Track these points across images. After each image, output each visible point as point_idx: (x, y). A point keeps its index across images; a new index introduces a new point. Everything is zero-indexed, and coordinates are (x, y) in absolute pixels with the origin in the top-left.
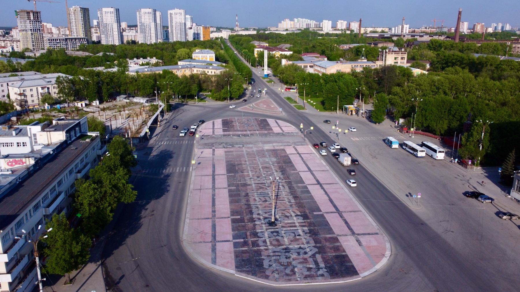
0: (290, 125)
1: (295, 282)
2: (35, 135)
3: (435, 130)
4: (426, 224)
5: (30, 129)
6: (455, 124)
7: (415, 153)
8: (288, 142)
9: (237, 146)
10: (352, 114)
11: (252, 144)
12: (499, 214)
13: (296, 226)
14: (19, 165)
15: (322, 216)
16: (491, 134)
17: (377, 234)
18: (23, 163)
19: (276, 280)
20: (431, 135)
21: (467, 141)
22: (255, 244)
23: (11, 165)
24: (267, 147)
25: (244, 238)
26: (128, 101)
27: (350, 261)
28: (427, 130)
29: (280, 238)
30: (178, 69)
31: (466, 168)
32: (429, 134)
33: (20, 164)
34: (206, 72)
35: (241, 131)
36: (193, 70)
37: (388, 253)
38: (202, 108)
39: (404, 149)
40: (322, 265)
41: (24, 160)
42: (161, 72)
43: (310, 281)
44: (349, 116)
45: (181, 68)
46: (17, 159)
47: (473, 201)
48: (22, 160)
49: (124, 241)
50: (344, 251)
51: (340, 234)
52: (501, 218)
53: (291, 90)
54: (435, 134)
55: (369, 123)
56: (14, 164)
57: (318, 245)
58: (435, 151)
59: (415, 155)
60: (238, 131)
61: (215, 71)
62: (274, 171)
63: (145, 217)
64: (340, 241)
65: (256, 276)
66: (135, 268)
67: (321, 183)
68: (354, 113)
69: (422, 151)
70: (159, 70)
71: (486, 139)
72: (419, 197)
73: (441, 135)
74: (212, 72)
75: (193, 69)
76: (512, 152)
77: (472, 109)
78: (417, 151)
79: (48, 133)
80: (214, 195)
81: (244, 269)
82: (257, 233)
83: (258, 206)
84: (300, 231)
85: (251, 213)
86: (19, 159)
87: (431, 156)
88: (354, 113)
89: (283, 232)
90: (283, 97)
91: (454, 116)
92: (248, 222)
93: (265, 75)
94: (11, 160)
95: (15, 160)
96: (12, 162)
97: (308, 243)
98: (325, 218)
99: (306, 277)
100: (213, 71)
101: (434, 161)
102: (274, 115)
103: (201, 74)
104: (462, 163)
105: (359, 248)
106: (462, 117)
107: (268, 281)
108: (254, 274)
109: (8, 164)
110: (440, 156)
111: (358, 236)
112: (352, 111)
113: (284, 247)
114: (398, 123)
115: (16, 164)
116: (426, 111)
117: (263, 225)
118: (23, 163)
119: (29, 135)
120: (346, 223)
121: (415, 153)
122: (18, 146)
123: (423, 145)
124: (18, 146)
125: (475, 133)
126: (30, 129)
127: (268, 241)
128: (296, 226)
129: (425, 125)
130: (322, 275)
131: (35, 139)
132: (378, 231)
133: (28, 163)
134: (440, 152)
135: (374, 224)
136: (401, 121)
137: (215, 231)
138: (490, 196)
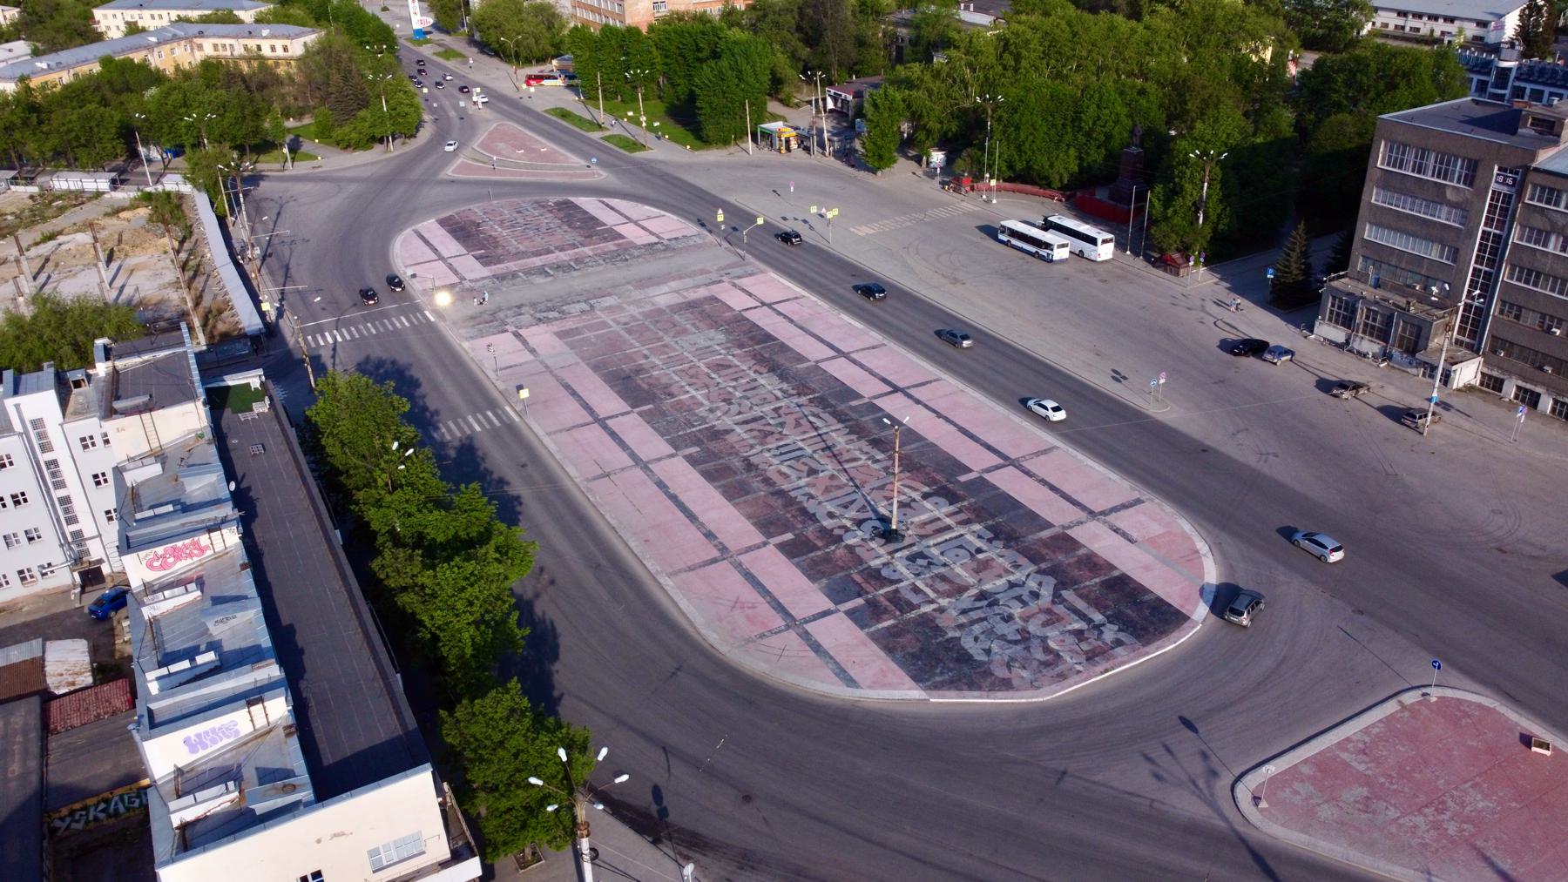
0: (656, 211)
1: (1076, 678)
2: (38, 424)
3: (1046, 178)
4: (1215, 451)
5: (17, 406)
6: (1096, 156)
7: (1043, 252)
8: (703, 272)
9: (575, 308)
10: (788, 149)
11: (610, 295)
12: (1325, 386)
13: (948, 528)
14: (189, 561)
15: (633, 406)
16: (1224, 183)
17: (1138, 501)
18: (202, 550)
19: (1033, 685)
20: (1036, 189)
21: (1166, 206)
22: (895, 598)
23: (162, 567)
24: (663, 297)
25: (859, 595)
26: (34, 189)
27: (1146, 591)
28: (1022, 177)
29: (942, 570)
30: (150, 47)
31: (1177, 274)
32: (1029, 187)
33: (191, 556)
34: (266, 52)
35: (537, 254)
36: (200, 47)
37: (1202, 546)
38: (328, 185)
39: (1001, 242)
40: (1098, 617)
41: (204, 539)
42: (96, 68)
43: (1107, 665)
44: (784, 157)
45: (159, 44)
46: (179, 544)
47: (1251, 362)
48: (196, 544)
49: (552, 687)
50: (1113, 567)
51: (1066, 522)
52: (1335, 396)
53: (546, 82)
54: (1049, 185)
55: (851, 170)
56: (171, 560)
57: (1043, 566)
58: (1093, 241)
59: (1041, 258)
60: (520, 255)
61: (287, 42)
62: (754, 376)
63: (537, 595)
64: (1082, 541)
65: (980, 688)
66: (663, 758)
67: (901, 385)
68: (794, 145)
69: (1063, 246)
70: (86, 61)
71: (1215, 198)
72: (1162, 381)
73: (1063, 188)
74: (273, 48)
75: (198, 41)
76: (1296, 229)
77: (1130, 116)
78: (1048, 246)
79: (146, 416)
80: (661, 485)
81: (938, 679)
82: (878, 571)
83: (807, 490)
84: (969, 537)
85: (812, 518)
86: (187, 541)
87: (1081, 254)
88: (794, 145)
89: (935, 552)
90: (539, 109)
91: (1088, 135)
92: (827, 546)
93: (418, 32)
94: (160, 550)
95: (174, 549)
96: (163, 556)
97: (1017, 566)
98: (995, 488)
99: (1091, 657)
100: (279, 44)
101: (1093, 266)
102: (575, 180)
103: (248, 60)
104: (1163, 262)
105: (1132, 547)
106: (1109, 137)
107: (1011, 693)
108: (973, 686)
109: (150, 566)
110: (1105, 251)
111: (1108, 518)
112: (788, 141)
113: (974, 591)
114: (928, 163)
115: (178, 558)
116: (1017, 128)
117: (873, 545)
118: (202, 550)
119: (18, 427)
120: (1043, 482)
121: (1043, 252)
122: (98, 483)
123: (1048, 226)
124: (98, 483)
125: (1188, 187)
126: (17, 406)
127: (920, 584)
128: (948, 528)
129: (1019, 166)
130: (1119, 643)
131: (41, 436)
132: (1136, 495)
133: (219, 547)
134: (1104, 241)
135: (1114, 476)
136: (938, 157)
137: (768, 593)
138: (1286, 345)
